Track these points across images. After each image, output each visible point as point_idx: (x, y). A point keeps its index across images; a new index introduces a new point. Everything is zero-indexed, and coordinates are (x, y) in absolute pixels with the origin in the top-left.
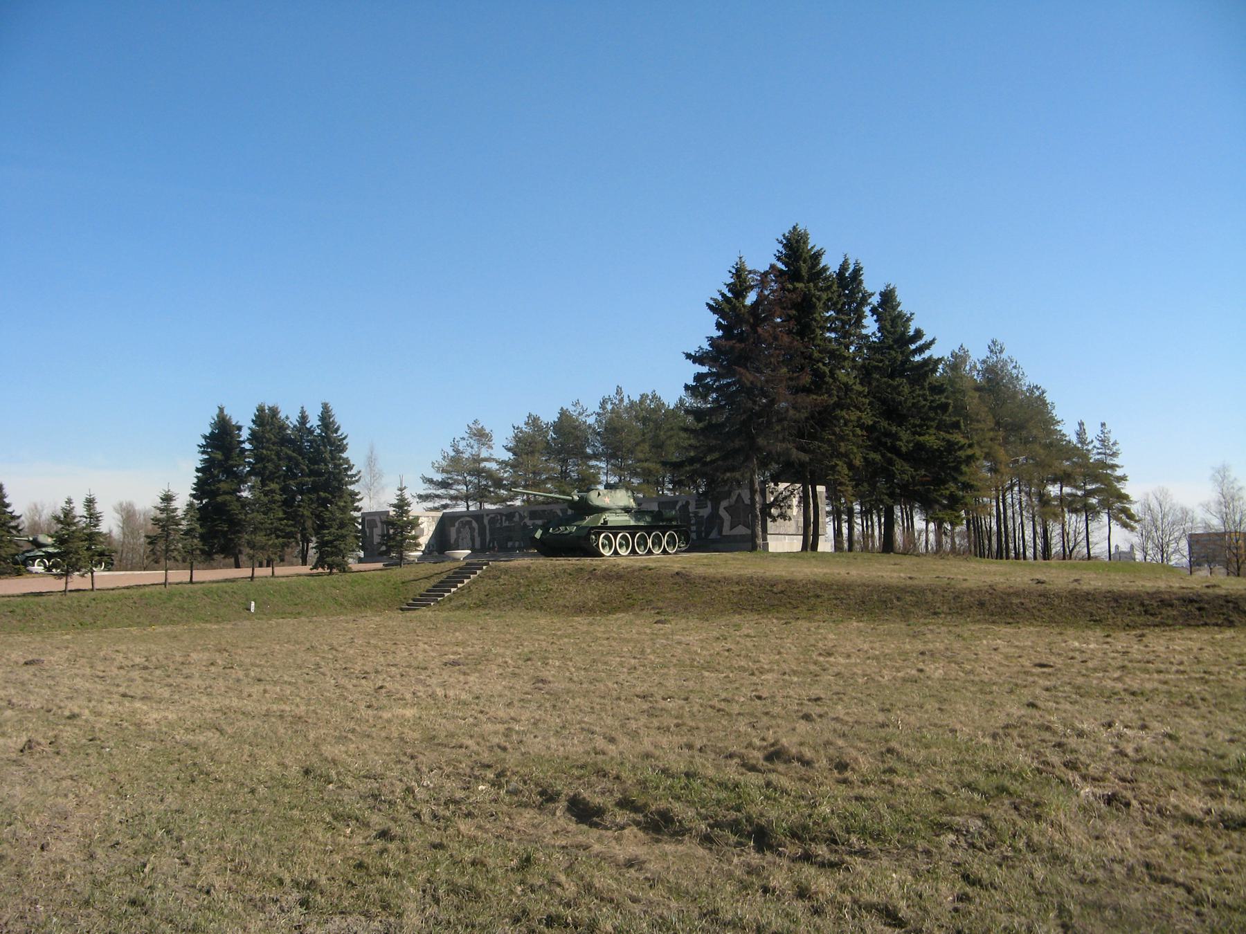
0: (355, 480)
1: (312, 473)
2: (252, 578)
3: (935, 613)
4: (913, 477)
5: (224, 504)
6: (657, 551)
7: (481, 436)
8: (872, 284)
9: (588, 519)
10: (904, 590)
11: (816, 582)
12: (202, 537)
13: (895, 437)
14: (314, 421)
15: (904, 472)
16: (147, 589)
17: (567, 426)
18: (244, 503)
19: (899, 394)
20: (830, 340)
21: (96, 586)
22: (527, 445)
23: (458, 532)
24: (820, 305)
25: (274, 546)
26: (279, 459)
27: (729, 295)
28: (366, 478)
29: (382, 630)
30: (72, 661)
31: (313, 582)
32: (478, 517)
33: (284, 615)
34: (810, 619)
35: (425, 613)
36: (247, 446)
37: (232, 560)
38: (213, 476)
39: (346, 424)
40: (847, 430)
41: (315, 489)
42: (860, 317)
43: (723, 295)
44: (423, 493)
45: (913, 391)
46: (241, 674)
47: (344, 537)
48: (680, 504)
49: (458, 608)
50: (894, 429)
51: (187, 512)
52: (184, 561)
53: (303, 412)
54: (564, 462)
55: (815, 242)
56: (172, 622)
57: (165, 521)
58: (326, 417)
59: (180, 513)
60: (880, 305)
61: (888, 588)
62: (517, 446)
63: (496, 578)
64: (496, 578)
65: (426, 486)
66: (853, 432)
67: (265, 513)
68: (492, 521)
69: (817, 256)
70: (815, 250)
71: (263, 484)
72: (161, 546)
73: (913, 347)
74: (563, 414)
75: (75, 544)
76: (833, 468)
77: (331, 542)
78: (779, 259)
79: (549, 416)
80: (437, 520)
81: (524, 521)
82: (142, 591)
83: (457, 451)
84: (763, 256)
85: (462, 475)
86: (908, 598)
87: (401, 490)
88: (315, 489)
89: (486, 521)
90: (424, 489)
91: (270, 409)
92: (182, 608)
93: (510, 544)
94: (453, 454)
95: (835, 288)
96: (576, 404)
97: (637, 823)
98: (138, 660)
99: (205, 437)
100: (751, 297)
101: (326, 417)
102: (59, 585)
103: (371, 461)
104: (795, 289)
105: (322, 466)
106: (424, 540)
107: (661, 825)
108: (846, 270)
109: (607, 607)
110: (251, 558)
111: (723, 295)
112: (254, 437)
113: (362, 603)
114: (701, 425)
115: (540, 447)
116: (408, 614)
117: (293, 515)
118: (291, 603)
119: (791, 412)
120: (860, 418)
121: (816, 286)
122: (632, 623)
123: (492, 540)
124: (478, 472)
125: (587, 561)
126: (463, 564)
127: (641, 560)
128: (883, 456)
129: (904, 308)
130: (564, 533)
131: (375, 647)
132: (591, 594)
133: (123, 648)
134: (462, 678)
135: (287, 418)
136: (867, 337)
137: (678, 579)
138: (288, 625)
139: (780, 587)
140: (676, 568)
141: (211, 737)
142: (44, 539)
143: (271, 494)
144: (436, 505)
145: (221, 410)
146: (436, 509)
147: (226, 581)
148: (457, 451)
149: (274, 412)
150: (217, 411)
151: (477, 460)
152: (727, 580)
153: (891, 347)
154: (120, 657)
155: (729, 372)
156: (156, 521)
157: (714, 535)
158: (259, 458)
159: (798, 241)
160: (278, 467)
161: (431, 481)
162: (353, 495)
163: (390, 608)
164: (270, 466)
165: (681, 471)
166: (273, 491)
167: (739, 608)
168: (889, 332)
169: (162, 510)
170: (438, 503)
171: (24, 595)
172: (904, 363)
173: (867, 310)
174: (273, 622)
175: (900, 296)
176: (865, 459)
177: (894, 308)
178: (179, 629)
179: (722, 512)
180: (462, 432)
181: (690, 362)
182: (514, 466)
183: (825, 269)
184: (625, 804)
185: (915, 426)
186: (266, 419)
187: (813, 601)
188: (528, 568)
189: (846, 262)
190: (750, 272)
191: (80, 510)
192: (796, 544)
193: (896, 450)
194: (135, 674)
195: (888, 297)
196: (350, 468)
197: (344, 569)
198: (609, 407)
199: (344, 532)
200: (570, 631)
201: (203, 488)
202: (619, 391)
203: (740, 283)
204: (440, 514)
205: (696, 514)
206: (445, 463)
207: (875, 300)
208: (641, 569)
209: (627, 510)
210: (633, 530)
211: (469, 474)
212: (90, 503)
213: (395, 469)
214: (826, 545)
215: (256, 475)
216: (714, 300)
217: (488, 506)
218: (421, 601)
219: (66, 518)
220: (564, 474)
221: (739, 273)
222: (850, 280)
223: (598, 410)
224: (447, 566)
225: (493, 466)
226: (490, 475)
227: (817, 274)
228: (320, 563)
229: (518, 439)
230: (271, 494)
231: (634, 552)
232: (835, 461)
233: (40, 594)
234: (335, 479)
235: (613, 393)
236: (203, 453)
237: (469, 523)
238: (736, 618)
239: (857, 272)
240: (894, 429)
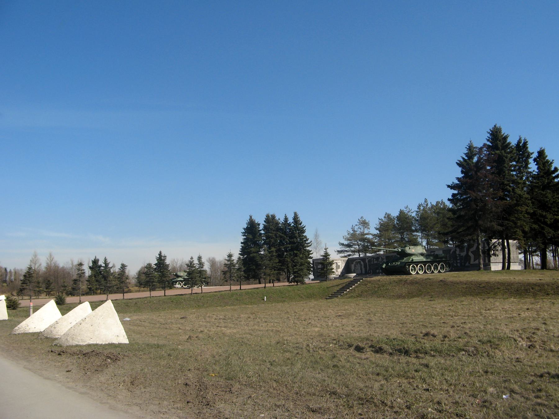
0: (309, 245)
1: (291, 243)
2: (265, 287)
3: (548, 294)
4: (554, 235)
5: (254, 257)
6: (436, 272)
7: (364, 224)
8: (533, 149)
9: (405, 259)
10: (535, 285)
11: (498, 282)
12: (244, 271)
13: (545, 217)
14: (291, 220)
15: (550, 233)
16: (223, 293)
17: (403, 217)
18: (262, 257)
19: (546, 197)
20: (513, 175)
21: (203, 292)
22: (386, 227)
23: (355, 266)
24: (507, 160)
25: (273, 274)
26: (276, 237)
27: (466, 158)
28: (314, 244)
29: (316, 306)
30: (198, 317)
31: (289, 289)
32: (363, 259)
33: (278, 302)
34: (493, 298)
35: (336, 300)
36: (262, 232)
37: (258, 281)
38: (248, 245)
39: (305, 221)
40: (521, 216)
41: (292, 250)
42: (527, 163)
43: (463, 158)
44: (340, 250)
45: (554, 196)
46: (259, 320)
47: (302, 270)
48: (452, 251)
49: (349, 298)
50: (544, 213)
51: (238, 261)
52: (237, 281)
53: (286, 217)
54: (402, 234)
55: (505, 131)
56: (233, 305)
57: (229, 265)
58: (296, 218)
59: (235, 261)
60: (538, 157)
61: (529, 284)
62: (380, 227)
63: (366, 285)
64: (366, 285)
65: (341, 246)
66: (524, 216)
67: (270, 261)
68: (369, 261)
69: (505, 138)
70: (505, 135)
71: (270, 248)
72: (228, 275)
73: (554, 175)
74: (401, 212)
75: (195, 275)
76: (515, 232)
77: (297, 272)
78: (488, 140)
79: (395, 214)
80: (345, 261)
81: (380, 261)
82: (221, 293)
83: (354, 231)
84: (481, 139)
85: (356, 241)
86: (537, 288)
87: (326, 249)
88: (292, 250)
89: (367, 261)
90: (340, 248)
91: (271, 215)
92: (237, 300)
93: (377, 271)
94: (352, 232)
95: (514, 151)
96: (407, 207)
97: (372, 351)
98: (221, 317)
99: (244, 229)
100: (475, 159)
101: (296, 218)
102: (189, 291)
103: (316, 236)
104: (496, 153)
105: (295, 240)
106: (340, 270)
107: (379, 350)
108: (520, 143)
109: (411, 295)
110: (265, 279)
111: (463, 158)
112: (265, 228)
113: (310, 296)
114: (456, 216)
115: (391, 227)
116: (328, 300)
117: (282, 262)
118: (281, 297)
119: (494, 209)
120: (527, 210)
121: (505, 151)
122: (419, 301)
124: (363, 240)
125: (404, 277)
126: (352, 280)
127: (429, 275)
128: (539, 225)
129: (549, 158)
130: (396, 265)
131: (312, 311)
132: (404, 290)
133: (216, 314)
134: (340, 320)
135: (279, 219)
136: (531, 172)
137: (441, 283)
138: (279, 305)
139: (483, 285)
140: (441, 278)
141: (249, 336)
142: (181, 274)
143: (274, 251)
144: (345, 255)
145: (251, 217)
146: (345, 257)
147: (254, 288)
148: (354, 231)
149: (273, 217)
150: (249, 218)
151: (363, 234)
152: (461, 283)
153: (542, 176)
154: (215, 316)
155: (465, 193)
156: (226, 265)
157: (467, 264)
158: (268, 237)
159: (496, 132)
160: (276, 241)
161: (343, 244)
162: (309, 252)
163: (322, 298)
164: (273, 240)
165: (443, 236)
166: (272, 252)
167: (465, 294)
168: (542, 170)
169: (228, 261)
170: (346, 254)
171: (176, 295)
172: (548, 183)
173: (531, 160)
174: (273, 304)
175: (547, 153)
176: (531, 227)
177: (544, 158)
178: (236, 307)
179: (470, 254)
180: (356, 222)
181: (449, 189)
182: (379, 236)
183: (509, 143)
184: (371, 346)
185: (554, 211)
186: (270, 220)
187: (496, 290)
188: (379, 280)
189: (520, 139)
190: (474, 148)
191: (196, 262)
192: (499, 267)
193: (545, 223)
194: (221, 321)
195: (541, 153)
196: (307, 240)
197: (303, 283)
198: (422, 208)
199: (302, 267)
200: (392, 304)
201: (244, 251)
202: (426, 201)
203: (471, 151)
204: (347, 259)
205: (459, 255)
206: (349, 236)
207: (535, 155)
208: (426, 279)
209: (422, 254)
210: (425, 263)
211: (360, 241)
212: (200, 258)
213: (327, 241)
214: (515, 267)
215: (267, 244)
216: (459, 161)
217: (368, 255)
218: (334, 295)
219: (190, 265)
220: (402, 239)
221: (470, 148)
222: (522, 147)
223: (417, 210)
224: (346, 280)
225: (370, 237)
226: (369, 241)
227: (506, 146)
228: (294, 280)
229: (381, 225)
230: (274, 251)
231: (425, 272)
232: (516, 229)
233: (182, 295)
234: (301, 245)
235: (423, 202)
236: (244, 236)
237: (360, 262)
238: (463, 298)
239: (525, 143)
240: (544, 213)
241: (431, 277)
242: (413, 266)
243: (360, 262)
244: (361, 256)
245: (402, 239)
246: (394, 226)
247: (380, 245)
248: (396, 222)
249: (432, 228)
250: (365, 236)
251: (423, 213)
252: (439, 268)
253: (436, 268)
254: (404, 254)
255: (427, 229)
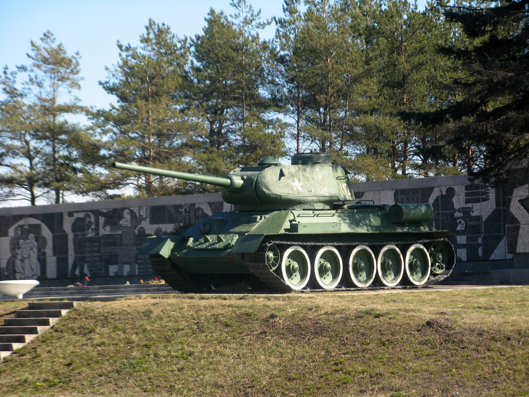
6: (391, 281)
7: (57, 63)
17: (220, 45)
32: (52, 218)
54: (216, 113)
62: (126, 83)
63: (87, 332)
64: (87, 332)
68: (79, 226)
74: (214, 21)
79: (188, 27)
89: (67, 225)
93: (113, 269)
114: (477, 42)
115: (171, 84)
123: (80, 261)
124: (52, 133)
125: (259, 301)
127: (362, 299)
137: (431, 335)
140: (427, 313)
148: (12, 92)
151: (50, 109)
157: (500, 252)
165: (440, 129)
182: (121, 121)
188: (148, 314)
205: (466, 212)
208: (359, 316)
209: (334, 204)
211: (36, 136)
220: (217, 137)
225: (80, 121)
226: (74, 138)
229: (129, 71)
237: (36, 229)
241: (380, 308)
242: (295, 256)
243: (36, 229)
244: (40, 202)
245: (217, 137)
246: (185, 77)
247: (123, 155)
248: (192, 61)
249: (344, 94)
250: (61, 118)
251: (307, 31)
252: (378, 265)
253: (393, 264)
254: (255, 201)
255: (321, 98)
